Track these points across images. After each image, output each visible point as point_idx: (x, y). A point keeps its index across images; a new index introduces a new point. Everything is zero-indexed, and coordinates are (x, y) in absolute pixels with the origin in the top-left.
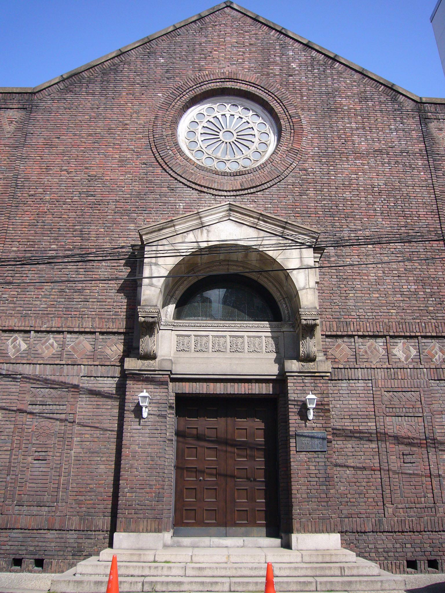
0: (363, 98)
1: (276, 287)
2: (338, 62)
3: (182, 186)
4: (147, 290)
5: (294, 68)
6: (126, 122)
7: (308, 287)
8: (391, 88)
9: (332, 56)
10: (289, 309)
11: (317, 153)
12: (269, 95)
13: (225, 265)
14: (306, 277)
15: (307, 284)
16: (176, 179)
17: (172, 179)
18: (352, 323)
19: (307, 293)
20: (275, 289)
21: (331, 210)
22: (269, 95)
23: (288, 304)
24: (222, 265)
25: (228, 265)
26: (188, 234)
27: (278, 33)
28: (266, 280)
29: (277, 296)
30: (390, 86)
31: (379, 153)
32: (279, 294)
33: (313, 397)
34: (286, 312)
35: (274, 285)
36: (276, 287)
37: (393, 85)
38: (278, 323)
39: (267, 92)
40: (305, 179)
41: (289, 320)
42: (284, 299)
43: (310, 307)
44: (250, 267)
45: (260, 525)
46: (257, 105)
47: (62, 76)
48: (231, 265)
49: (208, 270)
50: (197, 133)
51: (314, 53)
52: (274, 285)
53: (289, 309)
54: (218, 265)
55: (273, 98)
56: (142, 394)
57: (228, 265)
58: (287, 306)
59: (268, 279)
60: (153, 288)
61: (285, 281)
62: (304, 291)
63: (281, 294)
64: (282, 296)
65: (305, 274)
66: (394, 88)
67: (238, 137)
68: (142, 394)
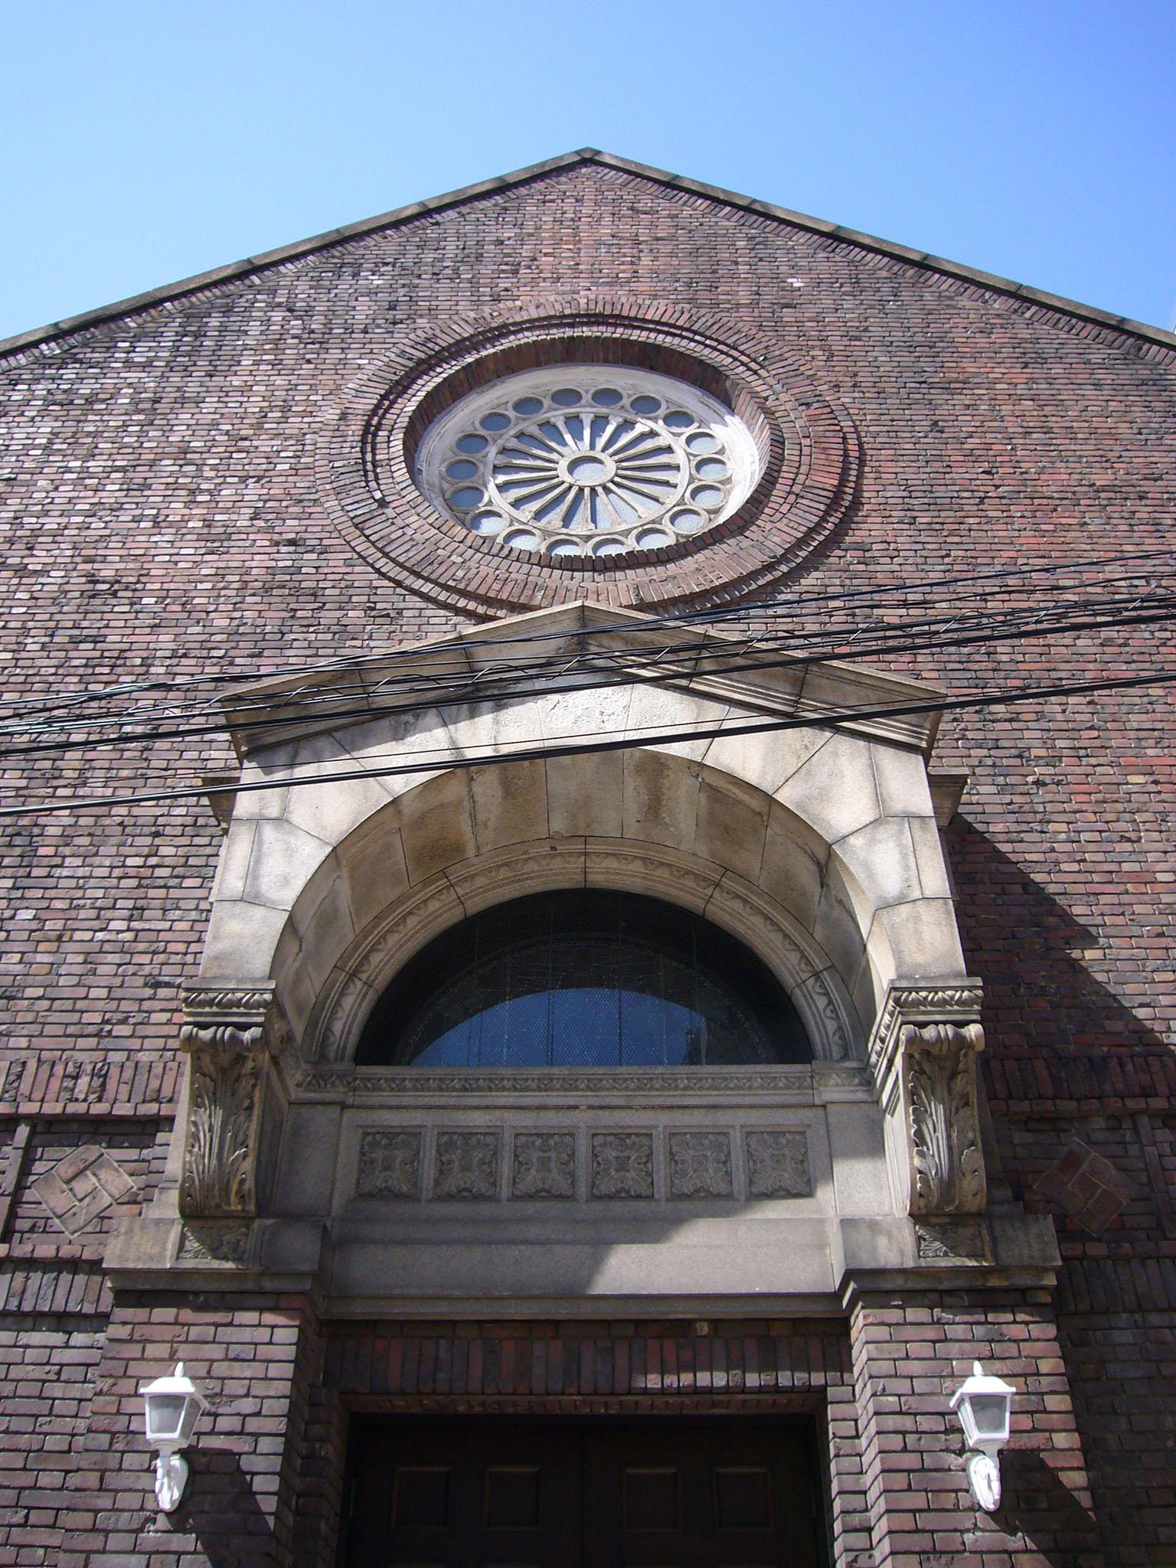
0: (1032, 358)
1: (781, 930)
2: (936, 270)
3: (418, 605)
4: (232, 916)
5: (799, 289)
6: (242, 432)
7: (917, 894)
8: (1120, 327)
9: (916, 258)
10: (843, 1014)
11: (900, 501)
12: (722, 352)
13: (571, 855)
14: (905, 857)
15: (914, 882)
16: (399, 584)
17: (386, 583)
18: (1113, 1063)
19: (917, 919)
20: (776, 938)
21: (971, 666)
22: (722, 352)
23: (835, 996)
24: (562, 855)
25: (586, 854)
26: (417, 717)
27: (741, 213)
28: (737, 905)
29: (785, 962)
30: (1113, 323)
31: (1112, 495)
32: (794, 957)
33: (996, 1386)
34: (831, 1026)
35: (773, 923)
36: (781, 930)
37: (1123, 320)
38: (798, 1067)
39: (715, 344)
40: (864, 575)
41: (845, 1057)
42: (816, 975)
43: (935, 970)
44: (669, 859)
45: (764, 773)
46: (684, 387)
47: (56, 325)
48: (598, 855)
49: (504, 873)
50: (481, 466)
51: (857, 254)
52: (773, 923)
53: (843, 1014)
54: (545, 857)
55: (735, 359)
56: (163, 1385)
57: (586, 854)
58: (830, 1002)
59: (745, 901)
60: (259, 912)
61: (816, 890)
62: (904, 910)
63: (803, 956)
64: (809, 963)
65: (899, 845)
66: (1127, 327)
67: (621, 472)
68: (163, 1385)
